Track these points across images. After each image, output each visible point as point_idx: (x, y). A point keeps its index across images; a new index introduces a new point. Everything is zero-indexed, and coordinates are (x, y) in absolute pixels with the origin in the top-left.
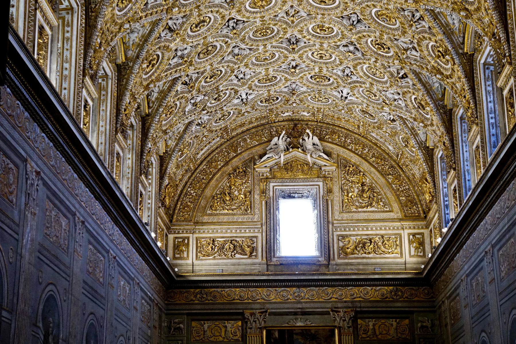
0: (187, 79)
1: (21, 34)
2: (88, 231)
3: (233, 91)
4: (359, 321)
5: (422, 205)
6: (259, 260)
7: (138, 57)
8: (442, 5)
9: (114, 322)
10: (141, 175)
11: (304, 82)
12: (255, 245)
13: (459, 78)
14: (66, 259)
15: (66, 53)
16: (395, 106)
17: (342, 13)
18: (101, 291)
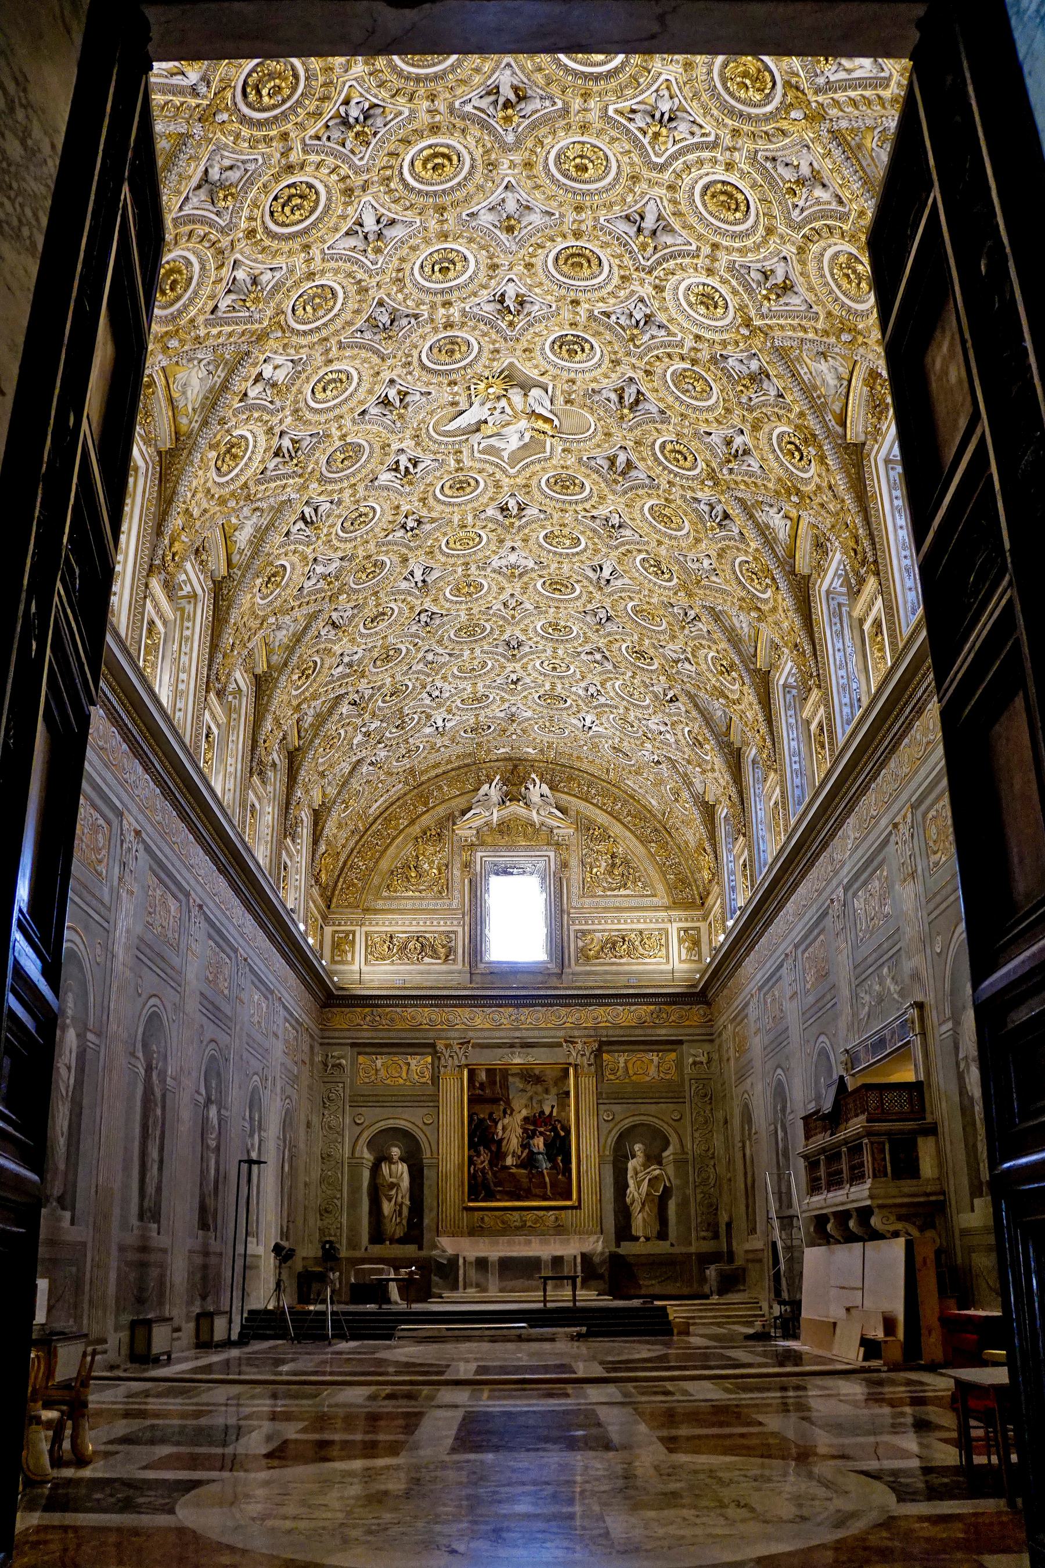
0: (356, 697)
1: (123, 633)
2: (208, 919)
3: (423, 716)
4: (605, 1056)
5: (698, 887)
6: (459, 966)
7: (285, 664)
8: (725, 601)
9: (245, 1054)
10: (285, 837)
11: (530, 703)
12: (453, 944)
13: (750, 704)
14: (176, 961)
15: (184, 659)
16: (661, 742)
17: (585, 606)
18: (227, 1009)
